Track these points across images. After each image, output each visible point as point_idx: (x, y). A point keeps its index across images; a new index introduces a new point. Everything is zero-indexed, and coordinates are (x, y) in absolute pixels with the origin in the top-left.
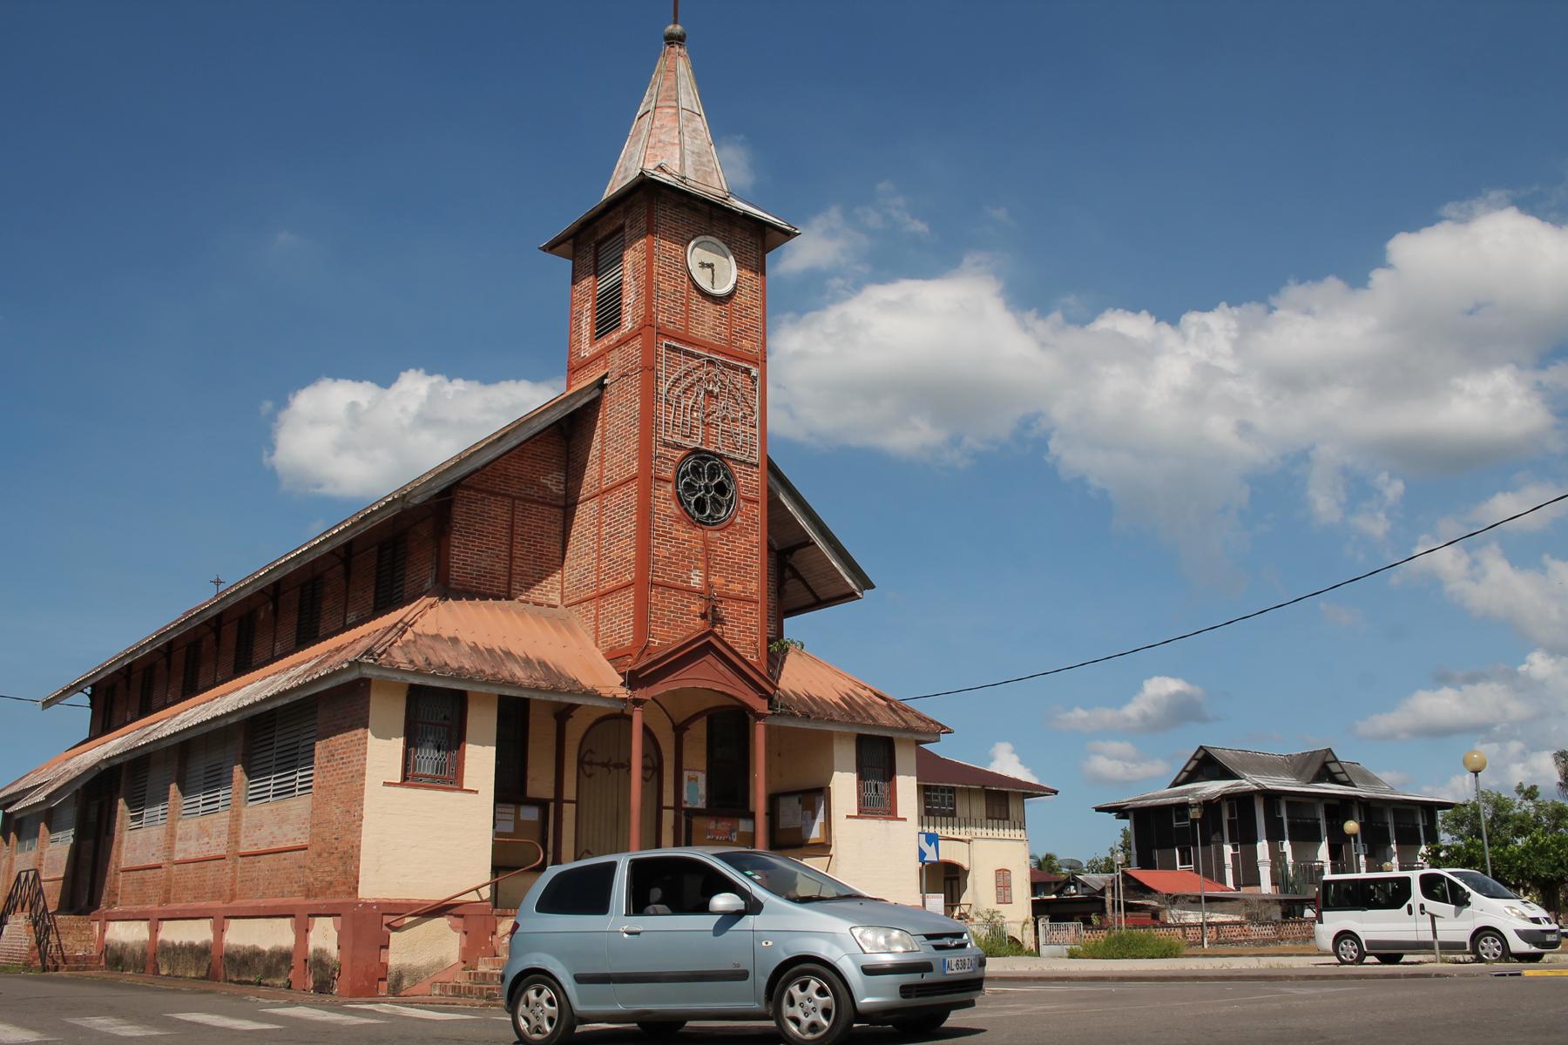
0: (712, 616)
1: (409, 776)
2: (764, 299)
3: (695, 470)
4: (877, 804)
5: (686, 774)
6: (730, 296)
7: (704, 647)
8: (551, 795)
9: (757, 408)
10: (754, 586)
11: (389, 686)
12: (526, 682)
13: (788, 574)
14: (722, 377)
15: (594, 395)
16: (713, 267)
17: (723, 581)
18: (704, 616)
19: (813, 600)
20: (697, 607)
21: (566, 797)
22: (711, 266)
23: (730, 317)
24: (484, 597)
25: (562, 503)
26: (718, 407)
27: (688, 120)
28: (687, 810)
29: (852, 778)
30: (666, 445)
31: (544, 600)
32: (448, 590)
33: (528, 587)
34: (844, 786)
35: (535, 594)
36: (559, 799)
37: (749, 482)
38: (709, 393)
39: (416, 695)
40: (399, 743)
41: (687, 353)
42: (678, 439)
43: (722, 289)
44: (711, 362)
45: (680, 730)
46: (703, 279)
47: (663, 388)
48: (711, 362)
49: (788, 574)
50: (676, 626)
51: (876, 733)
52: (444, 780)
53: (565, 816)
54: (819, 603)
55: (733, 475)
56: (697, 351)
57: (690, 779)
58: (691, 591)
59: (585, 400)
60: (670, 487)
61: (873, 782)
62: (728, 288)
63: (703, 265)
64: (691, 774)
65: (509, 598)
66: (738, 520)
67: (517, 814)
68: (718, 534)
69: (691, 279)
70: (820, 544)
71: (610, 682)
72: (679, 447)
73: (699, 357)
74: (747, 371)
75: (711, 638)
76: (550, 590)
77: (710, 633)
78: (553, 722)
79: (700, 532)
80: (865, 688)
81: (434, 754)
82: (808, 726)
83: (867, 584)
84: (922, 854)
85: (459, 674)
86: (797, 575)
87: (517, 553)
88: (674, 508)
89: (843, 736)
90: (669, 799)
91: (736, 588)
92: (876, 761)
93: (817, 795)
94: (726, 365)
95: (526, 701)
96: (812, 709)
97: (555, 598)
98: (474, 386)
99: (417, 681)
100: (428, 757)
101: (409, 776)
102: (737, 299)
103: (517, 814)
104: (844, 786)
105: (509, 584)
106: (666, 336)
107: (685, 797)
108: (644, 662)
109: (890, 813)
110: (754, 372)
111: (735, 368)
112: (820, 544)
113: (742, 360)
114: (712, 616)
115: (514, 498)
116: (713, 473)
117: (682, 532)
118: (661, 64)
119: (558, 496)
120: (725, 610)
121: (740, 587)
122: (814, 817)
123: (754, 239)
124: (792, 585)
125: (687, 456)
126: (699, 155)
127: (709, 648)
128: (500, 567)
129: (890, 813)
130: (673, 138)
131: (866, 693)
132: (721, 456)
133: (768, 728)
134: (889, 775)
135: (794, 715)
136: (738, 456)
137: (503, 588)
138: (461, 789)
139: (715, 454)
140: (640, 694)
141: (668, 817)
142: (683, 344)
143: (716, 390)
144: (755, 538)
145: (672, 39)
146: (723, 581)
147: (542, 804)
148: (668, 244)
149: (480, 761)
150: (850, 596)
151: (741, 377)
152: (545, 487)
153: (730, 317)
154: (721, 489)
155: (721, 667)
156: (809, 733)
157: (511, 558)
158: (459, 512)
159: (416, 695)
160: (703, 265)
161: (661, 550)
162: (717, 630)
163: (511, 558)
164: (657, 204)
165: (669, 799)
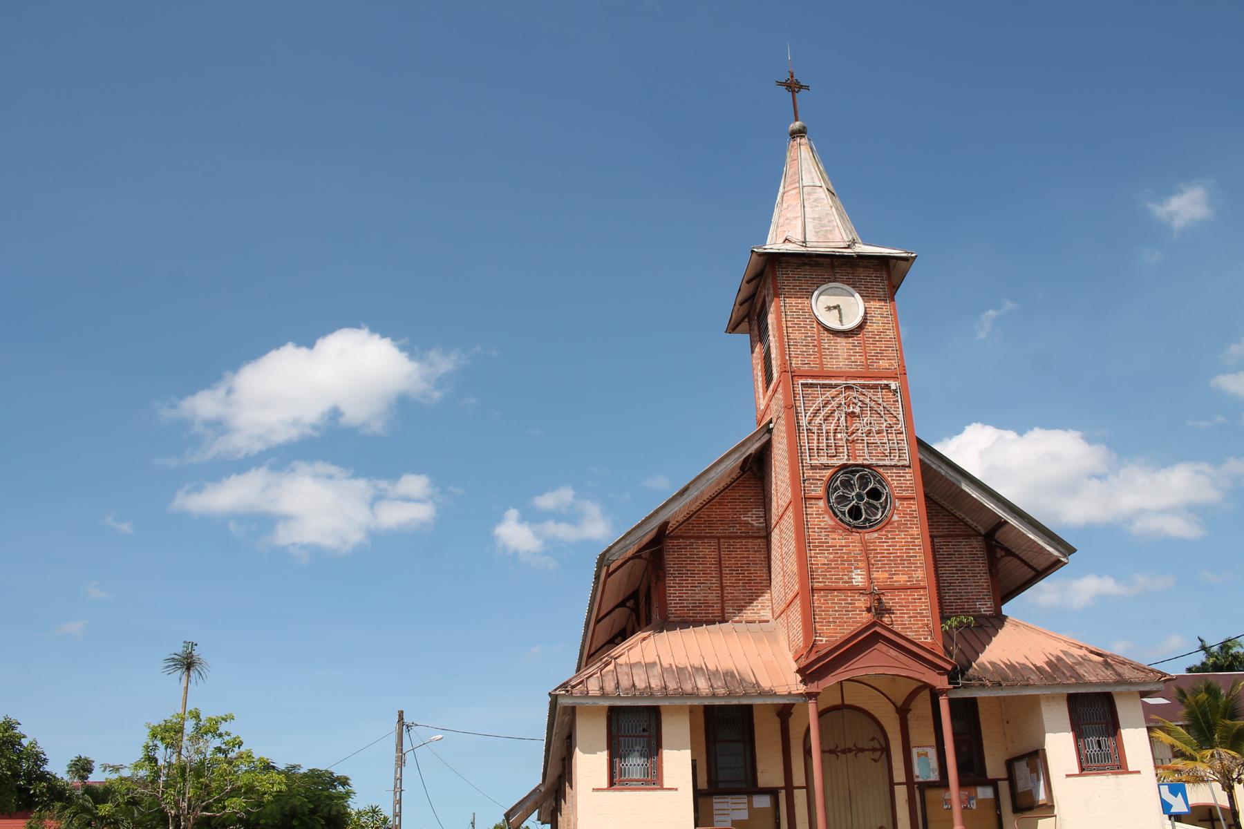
0: (880, 610)
1: (615, 780)
2: (896, 321)
3: (847, 484)
4: (1101, 756)
5: (915, 751)
6: (861, 327)
7: (866, 640)
8: (782, 784)
9: (901, 417)
10: (920, 574)
11: (592, 711)
12: (1093, 679)
13: (1000, 553)
14: (861, 398)
15: (764, 440)
16: (841, 307)
17: (886, 575)
18: (869, 610)
19: (1033, 573)
20: (862, 602)
21: (795, 784)
22: (837, 307)
23: (863, 345)
24: (697, 623)
25: (763, 533)
26: (860, 425)
27: (809, 194)
28: (920, 783)
29: (1068, 737)
30: (813, 467)
31: (756, 617)
32: (667, 624)
33: (740, 609)
34: (1060, 747)
35: (748, 614)
36: (789, 787)
37: (903, 484)
38: (852, 415)
39: (614, 714)
40: (603, 756)
41: (824, 386)
42: (824, 460)
43: (851, 323)
44: (848, 388)
45: (903, 712)
46: (831, 321)
47: (804, 422)
48: (848, 388)
49: (1000, 553)
50: (842, 621)
51: (1084, 691)
52: (647, 782)
53: (796, 800)
54: (1039, 574)
55: (885, 480)
56: (833, 382)
57: (919, 755)
58: (854, 589)
59: (757, 445)
60: (821, 503)
61: (1094, 739)
62: (857, 321)
63: (829, 308)
64: (920, 750)
65: (723, 621)
66: (895, 518)
67: (750, 803)
68: (876, 535)
69: (819, 323)
70: (1012, 521)
71: (794, 685)
72: (826, 467)
73: (831, 386)
74: (887, 387)
75: (878, 629)
76: (762, 608)
77: (874, 624)
78: (777, 720)
79: (856, 536)
80: (1081, 647)
81: (640, 761)
82: (1002, 693)
83: (1070, 550)
84: (1166, 807)
85: (649, 692)
86: (1009, 553)
87: (727, 582)
88: (828, 520)
89: (1051, 698)
90: (899, 775)
91: (901, 579)
92: (1094, 716)
93: (1036, 758)
94: (863, 386)
95: (749, 708)
96: (1011, 676)
97: (767, 614)
98: (1011, 435)
99: (607, 703)
100: (634, 764)
101: (1087, 765)
102: (869, 328)
103: (750, 803)
104: (1060, 747)
105: (723, 609)
106: (801, 376)
107: (917, 771)
108: (813, 657)
109: (1118, 765)
110: (893, 385)
111: (875, 387)
112: (1012, 521)
113: (881, 378)
114: (880, 610)
115: (719, 538)
116: (864, 481)
117: (838, 539)
118: (790, 155)
119: (759, 529)
120: (888, 600)
121: (905, 577)
122: (1039, 780)
123: (878, 274)
124: (1008, 563)
125: (837, 472)
126: (820, 219)
127: (875, 638)
128: (713, 597)
129: (1118, 765)
130: (807, 216)
131: (1077, 652)
132: (869, 466)
133: (952, 702)
134: (1112, 728)
135: (983, 686)
136: (887, 463)
137: (717, 613)
138: (662, 788)
139: (863, 466)
140: (813, 688)
141: (901, 793)
142: (820, 379)
143: (857, 410)
144: (915, 531)
145: (796, 134)
146: (886, 575)
147: (773, 792)
148: (793, 301)
149: (678, 763)
150: (1056, 564)
151: (879, 395)
152: (747, 523)
153: (863, 345)
154: (875, 494)
155: (893, 653)
156: (1020, 697)
157: (722, 588)
158: (671, 559)
159: (614, 714)
160: (829, 308)
161: (820, 559)
162: (886, 620)
163: (722, 588)
164: (779, 274)
165: (899, 775)
